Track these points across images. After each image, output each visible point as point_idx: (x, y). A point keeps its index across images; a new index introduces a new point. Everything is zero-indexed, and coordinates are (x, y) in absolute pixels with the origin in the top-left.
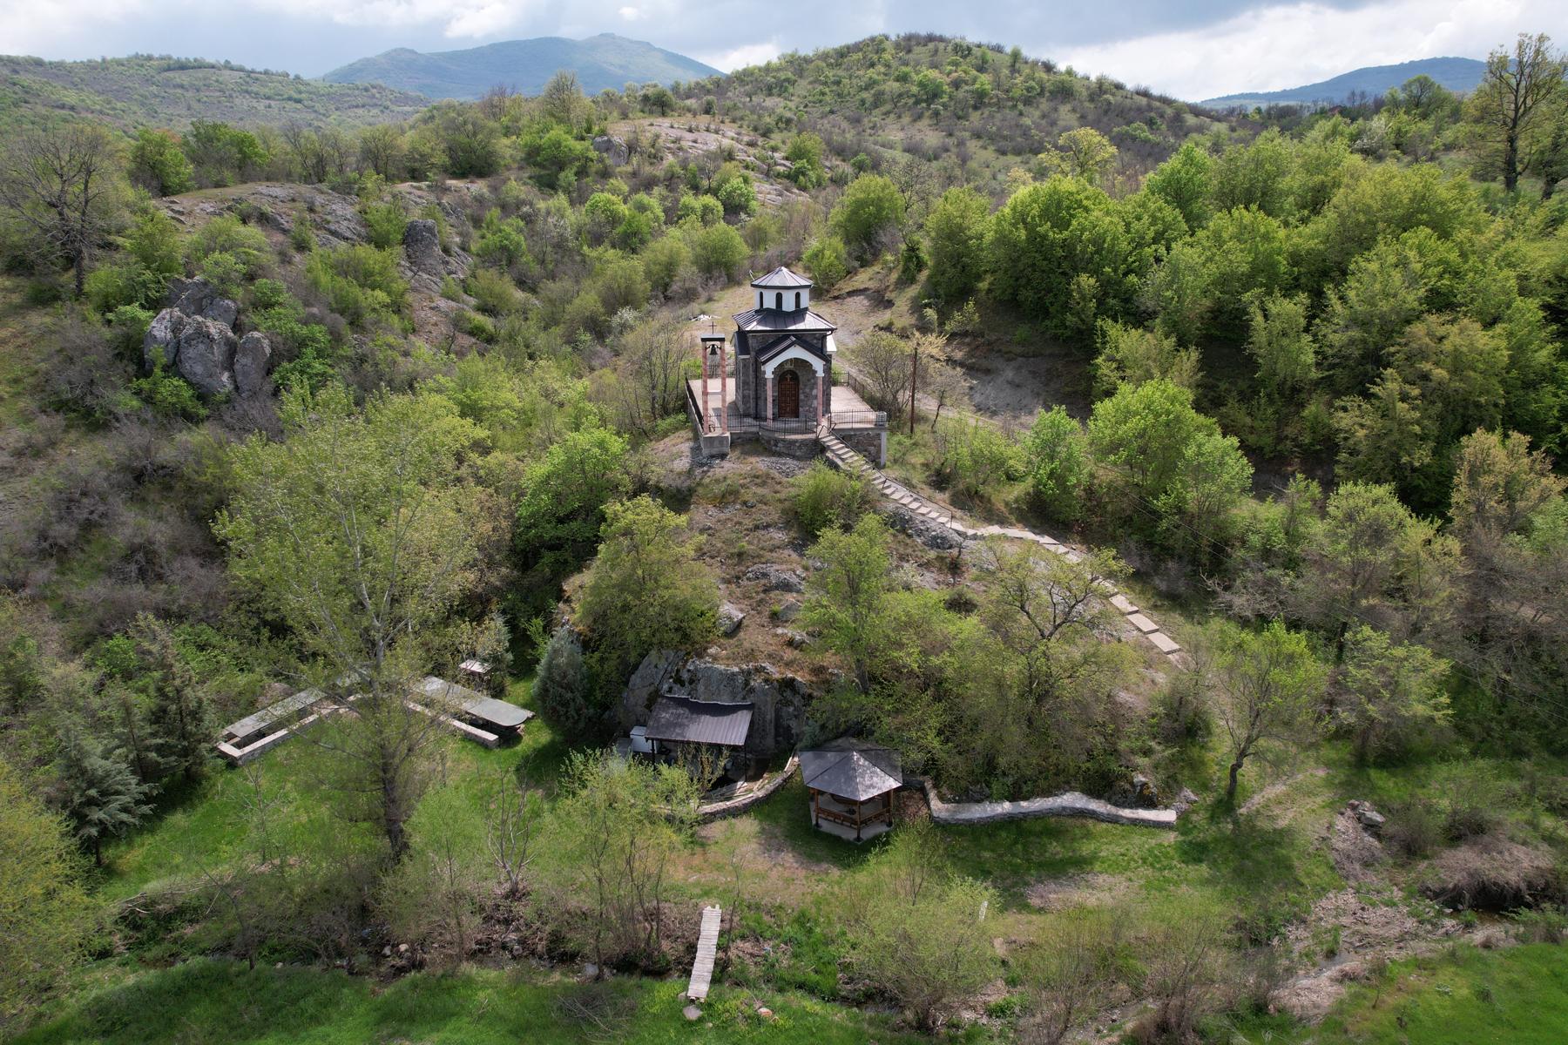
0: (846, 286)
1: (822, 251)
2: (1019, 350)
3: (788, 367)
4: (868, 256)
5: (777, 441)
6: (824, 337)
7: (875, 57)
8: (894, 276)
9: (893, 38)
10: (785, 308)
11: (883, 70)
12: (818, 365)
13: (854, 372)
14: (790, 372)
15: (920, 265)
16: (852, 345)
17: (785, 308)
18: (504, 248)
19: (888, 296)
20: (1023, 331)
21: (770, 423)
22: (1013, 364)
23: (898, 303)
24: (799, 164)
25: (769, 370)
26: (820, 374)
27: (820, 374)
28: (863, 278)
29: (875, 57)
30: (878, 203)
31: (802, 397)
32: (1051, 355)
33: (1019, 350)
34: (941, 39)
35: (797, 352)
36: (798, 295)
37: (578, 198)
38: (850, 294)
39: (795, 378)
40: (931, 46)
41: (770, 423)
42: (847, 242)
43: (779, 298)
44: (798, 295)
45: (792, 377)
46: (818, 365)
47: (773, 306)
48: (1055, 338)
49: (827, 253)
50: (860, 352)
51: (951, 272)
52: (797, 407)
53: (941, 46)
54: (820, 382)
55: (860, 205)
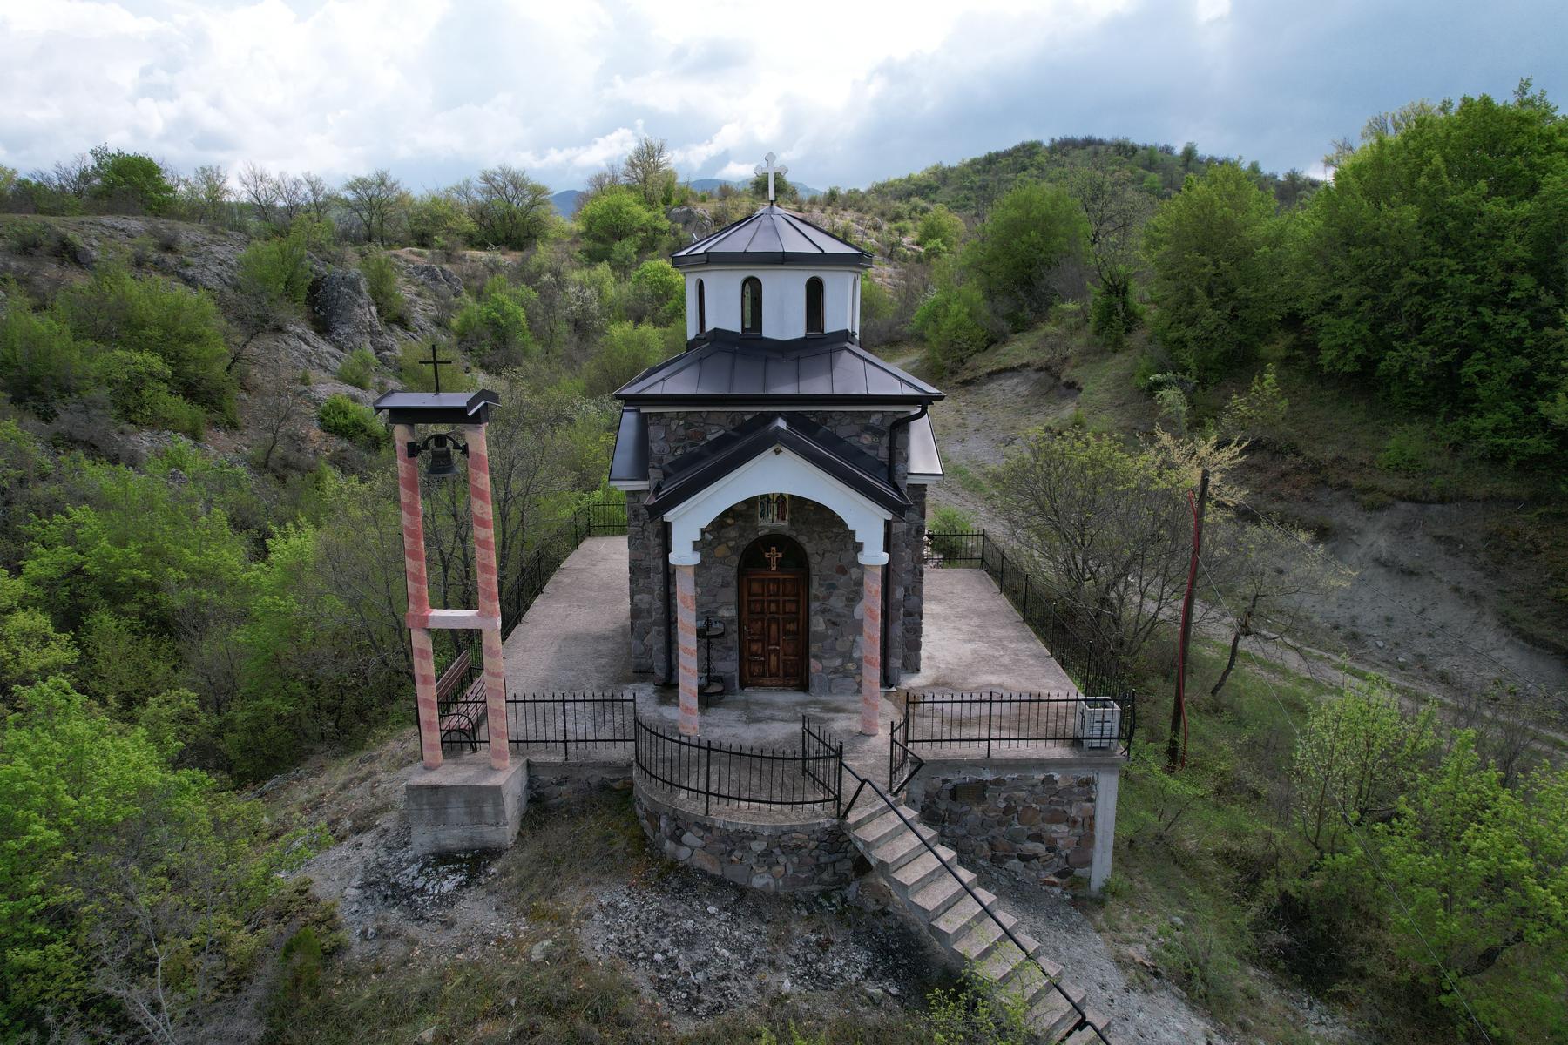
0: (987, 362)
1: (945, 305)
2: (1399, 484)
3: (769, 523)
4: (1026, 314)
5: (680, 825)
6: (901, 426)
7: (1027, 161)
8: (1080, 341)
9: (1047, 143)
10: (770, 331)
11: (1036, 172)
12: (865, 521)
13: (998, 530)
14: (775, 539)
15: (1132, 321)
16: (996, 464)
17: (770, 331)
18: (495, 324)
19: (1068, 374)
20: (1407, 439)
21: (686, 716)
22: (1385, 518)
23: (1088, 388)
24: (931, 244)
25: (689, 522)
26: (874, 555)
27: (874, 555)
28: (1021, 349)
29: (1027, 161)
30: (1046, 225)
31: (818, 624)
32: (1491, 499)
33: (1399, 484)
34: (1101, 143)
35: (778, 474)
36: (815, 291)
37: (622, 268)
38: (992, 375)
39: (796, 560)
40: (1090, 149)
41: (686, 716)
42: (990, 295)
43: (753, 291)
44: (815, 291)
45: (777, 564)
46: (865, 521)
47: (733, 324)
48: (1497, 458)
49: (954, 308)
50: (1012, 482)
51: (1211, 317)
52: (803, 655)
53: (1102, 149)
54: (873, 586)
55: (1015, 228)
